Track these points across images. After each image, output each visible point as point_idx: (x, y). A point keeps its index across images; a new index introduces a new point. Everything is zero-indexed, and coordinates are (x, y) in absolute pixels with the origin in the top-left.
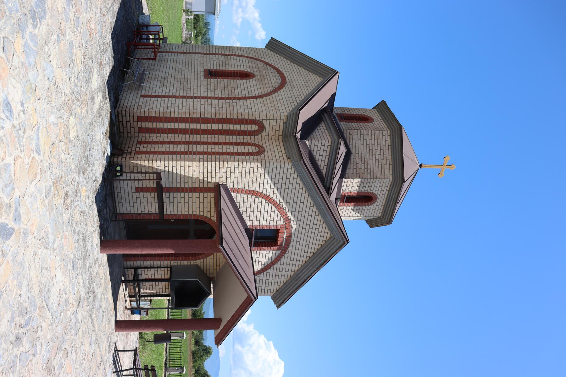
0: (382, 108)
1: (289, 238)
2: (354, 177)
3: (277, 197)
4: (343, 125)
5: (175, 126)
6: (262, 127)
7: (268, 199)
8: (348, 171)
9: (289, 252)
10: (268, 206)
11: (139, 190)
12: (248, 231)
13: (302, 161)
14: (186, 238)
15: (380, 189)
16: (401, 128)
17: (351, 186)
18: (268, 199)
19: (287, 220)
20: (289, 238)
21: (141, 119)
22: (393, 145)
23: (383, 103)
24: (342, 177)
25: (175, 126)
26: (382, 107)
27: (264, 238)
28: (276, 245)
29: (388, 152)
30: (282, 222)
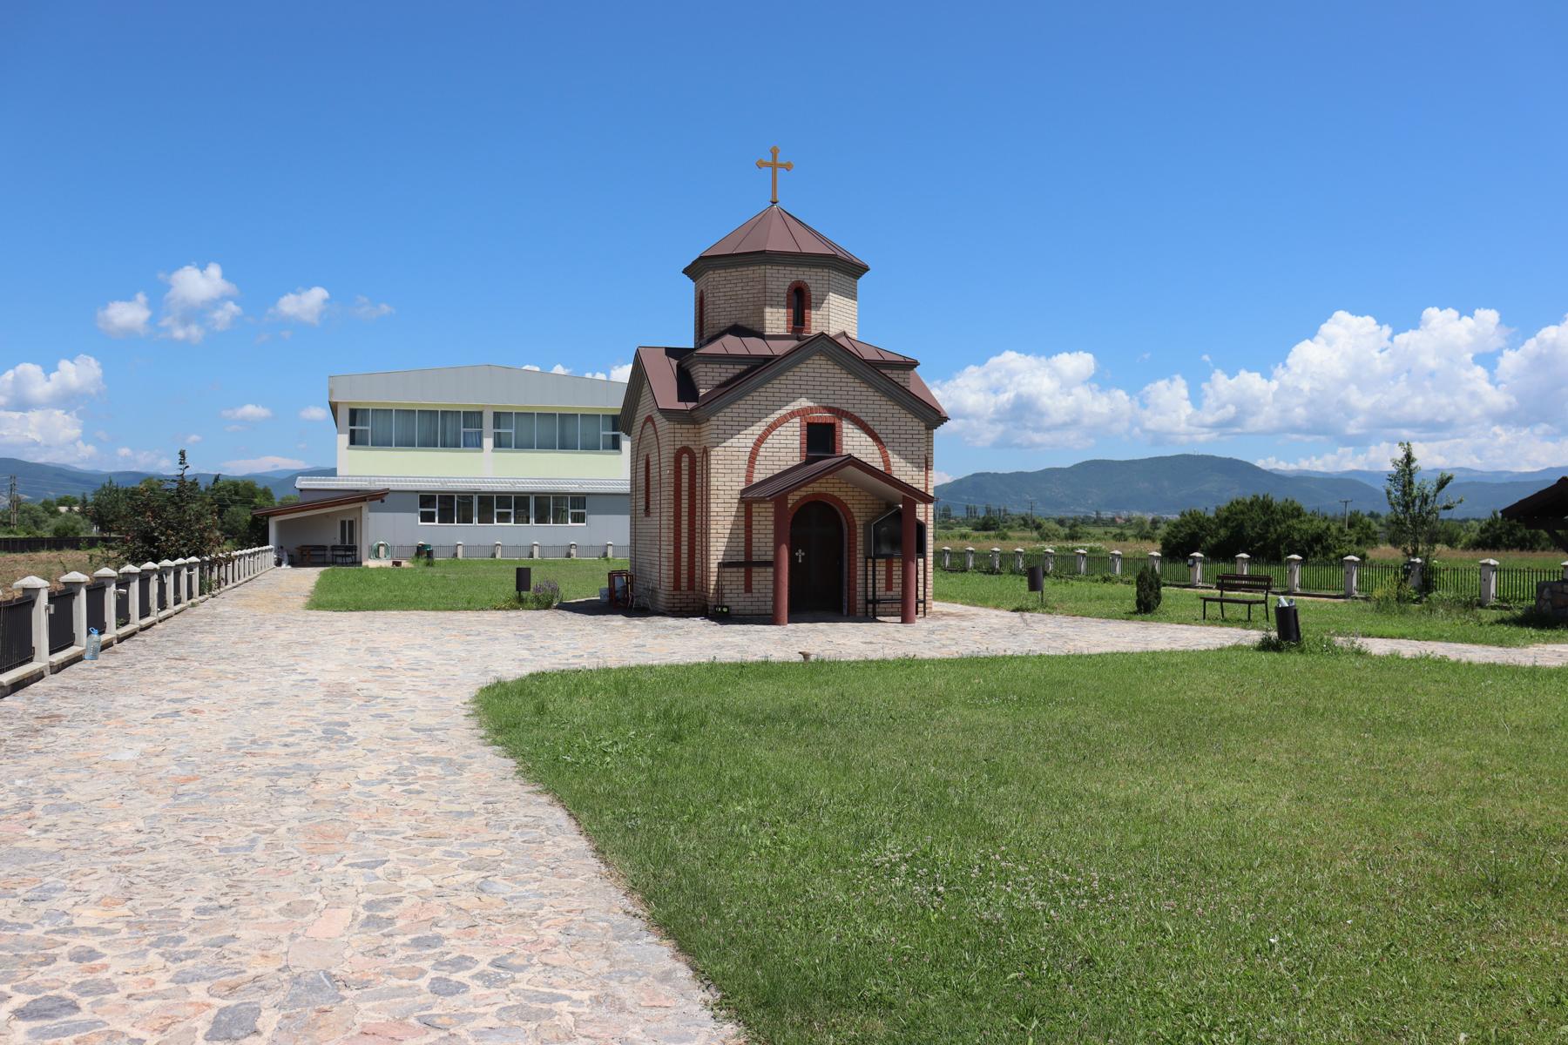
0: (693, 271)
1: (830, 410)
2: (762, 319)
3: (758, 429)
4: (706, 335)
5: (685, 549)
6: (685, 450)
7: (761, 440)
8: (756, 328)
9: (845, 407)
10: (770, 440)
11: (748, 588)
12: (809, 461)
13: (160, 626)
14: (1532, 549)
15: (781, 279)
16: (701, 258)
17: (776, 320)
18: (761, 440)
19: (793, 414)
20: (830, 410)
21: (677, 586)
22: (725, 267)
23: (686, 271)
24: (761, 336)
25: (685, 549)
26: (693, 271)
27: (820, 438)
28: (832, 426)
29: (733, 274)
30: (797, 420)
